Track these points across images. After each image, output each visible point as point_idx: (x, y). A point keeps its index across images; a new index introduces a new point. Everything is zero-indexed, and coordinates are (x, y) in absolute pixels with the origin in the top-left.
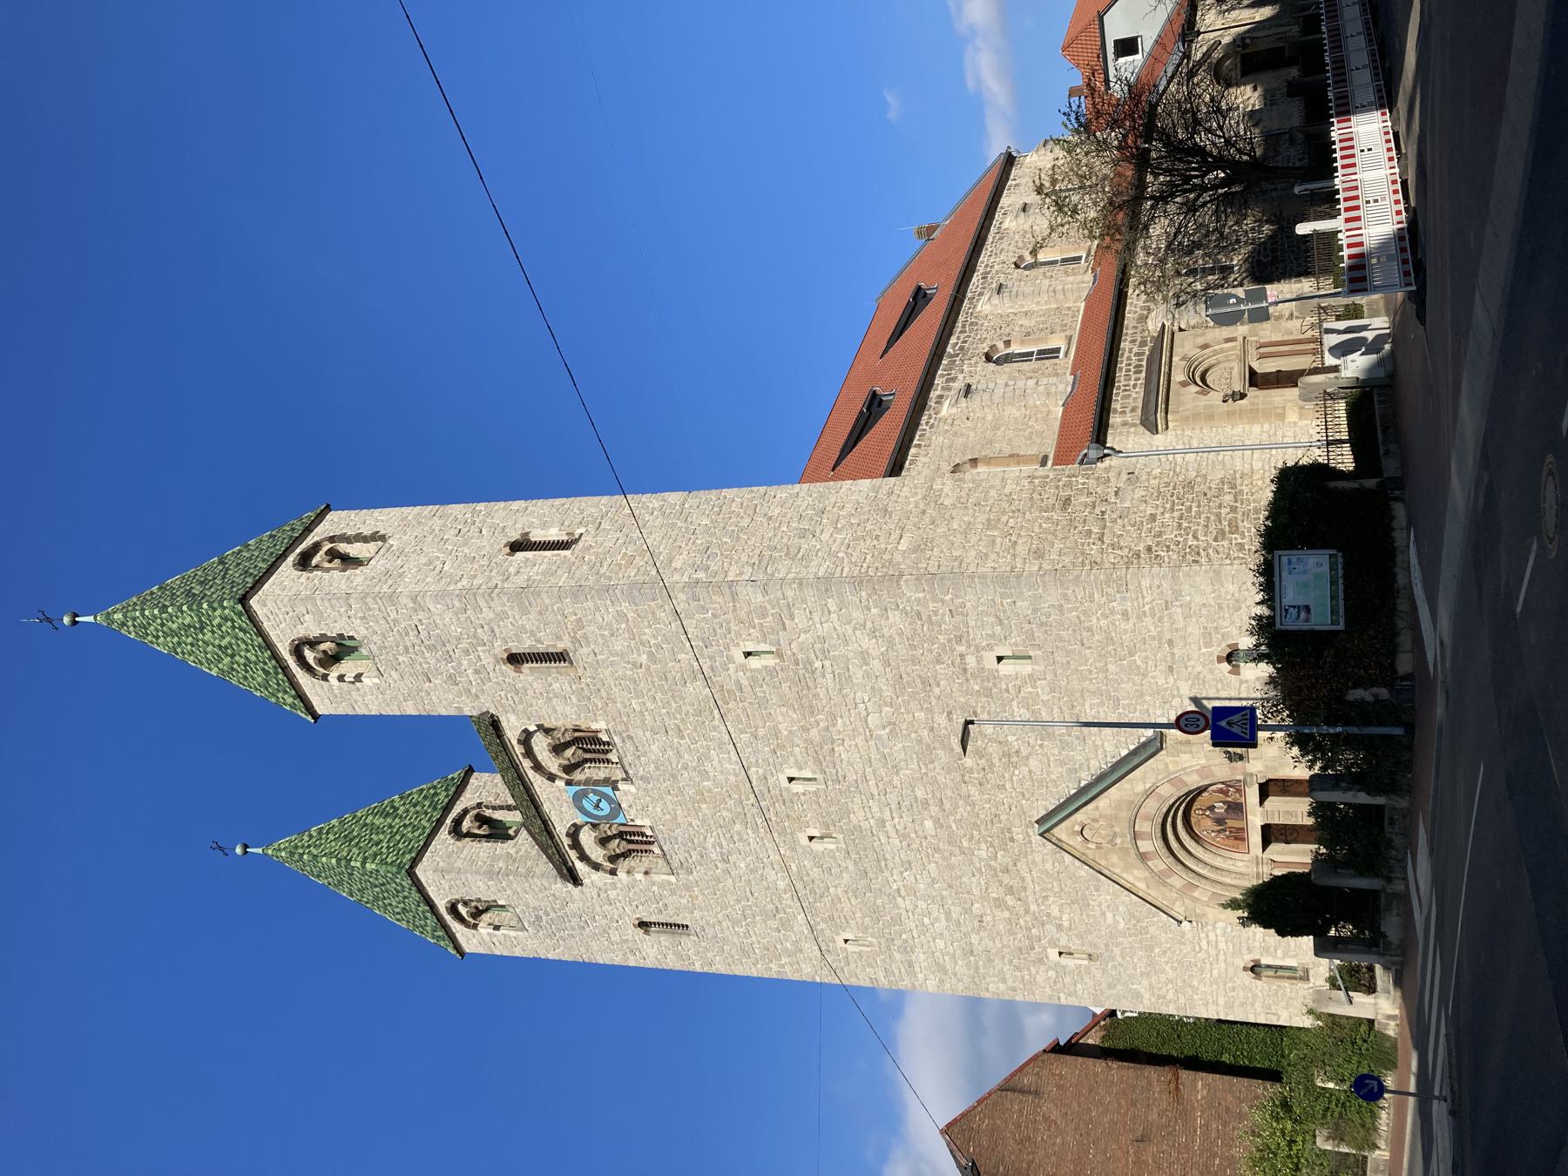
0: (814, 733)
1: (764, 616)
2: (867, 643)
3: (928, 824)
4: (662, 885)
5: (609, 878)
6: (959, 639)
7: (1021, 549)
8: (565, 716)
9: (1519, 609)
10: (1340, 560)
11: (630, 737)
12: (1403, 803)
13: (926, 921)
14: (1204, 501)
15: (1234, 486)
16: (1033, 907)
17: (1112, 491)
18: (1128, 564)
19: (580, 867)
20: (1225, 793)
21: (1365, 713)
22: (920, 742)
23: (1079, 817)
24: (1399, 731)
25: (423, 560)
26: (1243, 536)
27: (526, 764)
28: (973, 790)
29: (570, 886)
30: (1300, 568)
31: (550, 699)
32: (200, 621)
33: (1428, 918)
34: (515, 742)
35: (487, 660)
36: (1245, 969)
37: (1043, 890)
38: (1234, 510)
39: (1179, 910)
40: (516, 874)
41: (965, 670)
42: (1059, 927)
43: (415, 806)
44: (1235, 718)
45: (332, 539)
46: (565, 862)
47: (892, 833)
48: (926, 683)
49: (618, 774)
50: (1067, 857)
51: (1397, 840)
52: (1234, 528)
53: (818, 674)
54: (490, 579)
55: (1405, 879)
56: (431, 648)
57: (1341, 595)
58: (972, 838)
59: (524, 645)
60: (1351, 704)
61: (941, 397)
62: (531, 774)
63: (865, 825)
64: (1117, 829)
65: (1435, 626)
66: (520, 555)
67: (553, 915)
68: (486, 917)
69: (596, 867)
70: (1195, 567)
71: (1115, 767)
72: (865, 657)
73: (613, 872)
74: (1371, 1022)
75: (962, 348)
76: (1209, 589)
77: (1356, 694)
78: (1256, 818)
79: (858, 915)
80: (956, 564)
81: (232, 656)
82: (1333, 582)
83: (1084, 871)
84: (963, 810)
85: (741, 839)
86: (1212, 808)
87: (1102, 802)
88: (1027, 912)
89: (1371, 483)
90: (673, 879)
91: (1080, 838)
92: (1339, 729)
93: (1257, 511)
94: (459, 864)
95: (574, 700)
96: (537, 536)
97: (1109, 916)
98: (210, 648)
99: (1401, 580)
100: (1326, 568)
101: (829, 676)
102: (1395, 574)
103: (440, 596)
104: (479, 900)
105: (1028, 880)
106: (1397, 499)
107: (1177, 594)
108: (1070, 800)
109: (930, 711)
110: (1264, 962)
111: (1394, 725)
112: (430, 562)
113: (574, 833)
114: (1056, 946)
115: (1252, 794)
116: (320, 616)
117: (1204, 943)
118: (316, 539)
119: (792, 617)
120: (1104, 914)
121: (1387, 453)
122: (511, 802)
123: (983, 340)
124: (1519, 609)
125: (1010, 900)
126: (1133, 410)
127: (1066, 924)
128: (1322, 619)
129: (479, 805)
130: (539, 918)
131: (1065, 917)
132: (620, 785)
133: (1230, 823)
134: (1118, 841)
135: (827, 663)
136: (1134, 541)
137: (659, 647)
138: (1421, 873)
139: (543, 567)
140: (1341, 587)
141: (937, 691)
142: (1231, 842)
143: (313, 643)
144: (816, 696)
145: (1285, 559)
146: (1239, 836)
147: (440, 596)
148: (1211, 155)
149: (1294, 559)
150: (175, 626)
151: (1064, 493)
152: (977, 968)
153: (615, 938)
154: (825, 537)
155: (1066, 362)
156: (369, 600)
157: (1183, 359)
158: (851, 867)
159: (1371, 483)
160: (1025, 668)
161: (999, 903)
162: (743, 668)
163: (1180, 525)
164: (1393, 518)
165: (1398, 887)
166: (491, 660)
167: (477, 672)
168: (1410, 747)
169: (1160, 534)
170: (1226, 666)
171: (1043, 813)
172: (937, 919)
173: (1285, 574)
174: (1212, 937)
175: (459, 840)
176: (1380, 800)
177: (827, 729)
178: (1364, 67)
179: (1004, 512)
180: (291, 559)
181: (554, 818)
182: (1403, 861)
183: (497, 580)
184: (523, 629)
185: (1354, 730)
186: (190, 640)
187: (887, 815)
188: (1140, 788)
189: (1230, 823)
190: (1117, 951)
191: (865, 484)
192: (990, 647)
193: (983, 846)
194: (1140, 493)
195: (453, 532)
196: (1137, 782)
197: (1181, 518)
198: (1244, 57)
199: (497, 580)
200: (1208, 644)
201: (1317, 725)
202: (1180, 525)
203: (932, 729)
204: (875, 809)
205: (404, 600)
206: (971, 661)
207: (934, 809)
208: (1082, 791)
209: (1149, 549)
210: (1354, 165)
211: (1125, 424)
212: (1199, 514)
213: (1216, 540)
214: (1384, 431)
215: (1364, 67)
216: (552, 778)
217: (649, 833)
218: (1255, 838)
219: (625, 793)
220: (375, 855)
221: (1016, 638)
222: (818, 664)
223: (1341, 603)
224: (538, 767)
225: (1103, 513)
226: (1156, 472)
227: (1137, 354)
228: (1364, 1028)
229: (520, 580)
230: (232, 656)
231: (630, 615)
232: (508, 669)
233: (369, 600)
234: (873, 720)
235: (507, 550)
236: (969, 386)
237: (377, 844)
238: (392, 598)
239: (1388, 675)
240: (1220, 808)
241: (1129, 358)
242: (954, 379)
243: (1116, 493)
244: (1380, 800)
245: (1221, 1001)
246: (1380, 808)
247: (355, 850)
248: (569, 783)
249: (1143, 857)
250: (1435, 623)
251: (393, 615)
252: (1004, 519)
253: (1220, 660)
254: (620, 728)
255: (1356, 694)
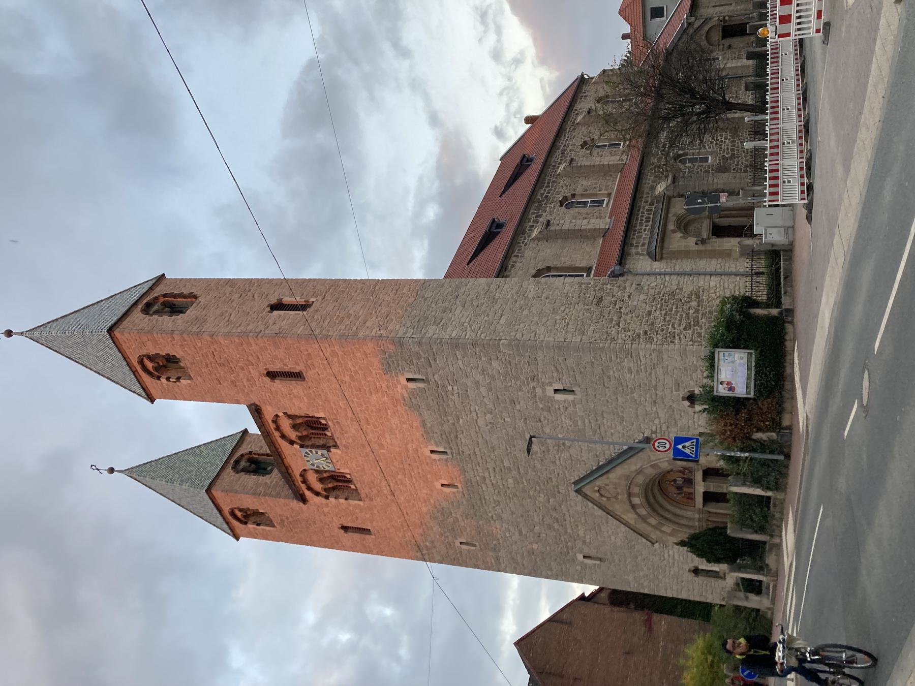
0: (446, 427)
1: (419, 359)
2: (480, 378)
3: (511, 481)
4: (355, 507)
5: (324, 500)
6: (533, 378)
7: (571, 328)
8: (301, 408)
9: (846, 434)
10: (754, 356)
11: (338, 423)
12: (780, 496)
13: (507, 535)
14: (680, 304)
15: (698, 297)
16: (569, 531)
17: (626, 295)
18: (633, 340)
19: (308, 494)
20: (683, 473)
21: (763, 447)
22: (508, 435)
23: (599, 483)
24: (781, 458)
25: (218, 312)
26: (701, 329)
27: (277, 434)
28: (538, 465)
29: (301, 504)
30: (730, 359)
31: (291, 399)
32: (85, 341)
33: (791, 565)
34: (270, 422)
35: (255, 374)
36: (689, 571)
37: (575, 521)
38: (697, 311)
39: (654, 535)
40: (270, 495)
41: (535, 396)
42: (584, 542)
43: (213, 451)
44: (687, 444)
45: (165, 296)
46: (298, 491)
47: (490, 486)
48: (513, 402)
49: (331, 443)
50: (590, 505)
51: (777, 515)
52: (697, 323)
53: (449, 393)
54: (257, 326)
55: (781, 536)
56: (221, 365)
57: (753, 377)
58: (536, 490)
59: (277, 367)
60: (755, 441)
61: (532, 226)
62: (280, 441)
63: (474, 480)
64: (619, 491)
65: (805, 404)
66: (276, 313)
67: (291, 519)
68: (252, 519)
69: (317, 494)
70: (672, 345)
71: (620, 455)
72: (477, 384)
73: (327, 497)
74: (758, 610)
75: (546, 197)
76: (679, 358)
77: (758, 435)
78: (700, 488)
79: (468, 529)
80: (533, 335)
81: (104, 362)
82: (749, 369)
83: (600, 513)
84: (531, 474)
85: (401, 483)
86: (675, 481)
87: (612, 476)
88: (566, 532)
89: (775, 312)
90: (361, 503)
91: (597, 494)
92: (747, 454)
93: (711, 313)
94: (237, 487)
95: (306, 400)
96: (287, 300)
97: (613, 538)
98: (91, 357)
99: (788, 370)
100: (746, 360)
101: (456, 395)
102: (785, 367)
103: (228, 335)
104: (248, 509)
105: (567, 516)
106: (788, 322)
107: (660, 359)
108: (593, 472)
109: (514, 417)
110: (700, 567)
111: (779, 454)
112: (222, 314)
113: (303, 474)
114: (581, 552)
115: (699, 476)
116: (155, 342)
117: (666, 555)
118: (156, 295)
119: (435, 360)
120: (609, 537)
121: (785, 293)
122: (269, 452)
123: (558, 193)
124: (846, 434)
125: (556, 526)
126: (643, 245)
127: (588, 541)
128: (741, 390)
129: (250, 453)
130: (282, 521)
131: (588, 537)
132: (332, 450)
133: (685, 490)
134: (620, 497)
135: (455, 388)
136: (637, 327)
137: (356, 372)
138: (789, 538)
139: (290, 321)
140: (753, 373)
141: (518, 407)
142: (685, 500)
143: (151, 358)
144: (448, 405)
145: (721, 354)
146: (690, 497)
147: (228, 335)
148: (698, 93)
149: (727, 354)
150: (70, 343)
151: (599, 294)
152: (536, 562)
153: (327, 534)
154: (458, 312)
155: (608, 204)
156: (185, 336)
157: (674, 215)
158: (465, 503)
159: (775, 312)
160: (570, 397)
161: (550, 527)
162: (406, 388)
163: (665, 319)
164: (786, 333)
165: (777, 540)
166: (257, 374)
167: (248, 380)
168: (787, 467)
169: (653, 324)
170: (687, 403)
171: (577, 478)
172: (514, 534)
173: (721, 362)
174: (671, 553)
175: (237, 473)
176: (769, 494)
177: (454, 424)
178: (648, 624)
179: (563, 305)
180: (140, 306)
181: (294, 467)
182: (780, 527)
183: (262, 327)
184: (276, 357)
185: (756, 455)
186: (79, 351)
187: (487, 475)
188: (633, 468)
189: (685, 490)
190: (616, 557)
191: (483, 281)
192: (550, 384)
193: (542, 495)
194: (642, 297)
195: (237, 296)
196: (633, 465)
197: (666, 314)
198: (724, 27)
199: (262, 327)
200: (678, 390)
201: (733, 450)
202: (665, 319)
203: (515, 428)
204: (480, 470)
205: (206, 337)
206: (539, 391)
207: (514, 473)
208: (600, 468)
209: (646, 332)
210: (778, 119)
211: (637, 253)
212: (677, 312)
213: (685, 329)
214: (785, 278)
215: (648, 624)
216: (292, 443)
217: (348, 476)
218: (699, 499)
219: (334, 454)
220: (188, 479)
221: (566, 379)
222: (450, 388)
223: (753, 382)
224: (283, 436)
225: (620, 308)
226: (653, 284)
227: (647, 210)
228: (754, 614)
229: (276, 329)
230: (104, 362)
231: (340, 353)
232: (267, 380)
233: (185, 336)
234: (481, 422)
235: (269, 309)
236: (549, 222)
237: (190, 472)
238: (199, 334)
239: (776, 425)
240: (680, 481)
241: (643, 213)
242: (540, 216)
243: (629, 296)
244: (769, 494)
245: (675, 588)
246: (769, 498)
247: (177, 476)
248: (302, 446)
249: (634, 507)
250: (804, 404)
251: (199, 344)
252: (562, 308)
253: (683, 399)
254: (332, 417)
255: (758, 435)
